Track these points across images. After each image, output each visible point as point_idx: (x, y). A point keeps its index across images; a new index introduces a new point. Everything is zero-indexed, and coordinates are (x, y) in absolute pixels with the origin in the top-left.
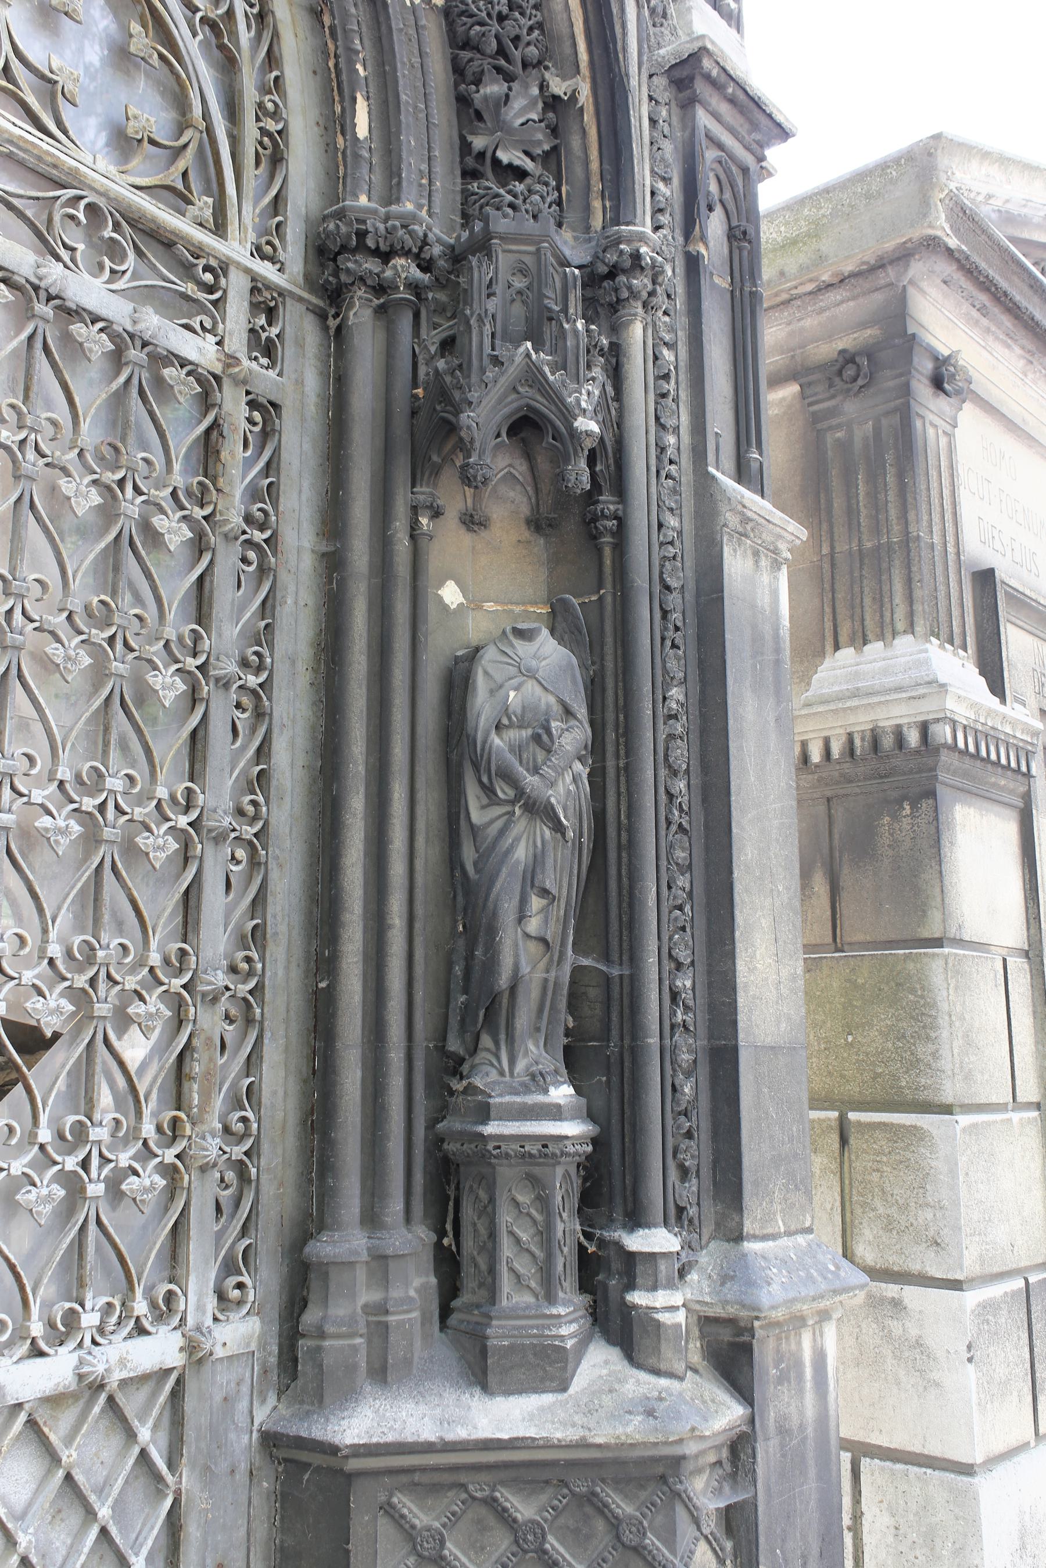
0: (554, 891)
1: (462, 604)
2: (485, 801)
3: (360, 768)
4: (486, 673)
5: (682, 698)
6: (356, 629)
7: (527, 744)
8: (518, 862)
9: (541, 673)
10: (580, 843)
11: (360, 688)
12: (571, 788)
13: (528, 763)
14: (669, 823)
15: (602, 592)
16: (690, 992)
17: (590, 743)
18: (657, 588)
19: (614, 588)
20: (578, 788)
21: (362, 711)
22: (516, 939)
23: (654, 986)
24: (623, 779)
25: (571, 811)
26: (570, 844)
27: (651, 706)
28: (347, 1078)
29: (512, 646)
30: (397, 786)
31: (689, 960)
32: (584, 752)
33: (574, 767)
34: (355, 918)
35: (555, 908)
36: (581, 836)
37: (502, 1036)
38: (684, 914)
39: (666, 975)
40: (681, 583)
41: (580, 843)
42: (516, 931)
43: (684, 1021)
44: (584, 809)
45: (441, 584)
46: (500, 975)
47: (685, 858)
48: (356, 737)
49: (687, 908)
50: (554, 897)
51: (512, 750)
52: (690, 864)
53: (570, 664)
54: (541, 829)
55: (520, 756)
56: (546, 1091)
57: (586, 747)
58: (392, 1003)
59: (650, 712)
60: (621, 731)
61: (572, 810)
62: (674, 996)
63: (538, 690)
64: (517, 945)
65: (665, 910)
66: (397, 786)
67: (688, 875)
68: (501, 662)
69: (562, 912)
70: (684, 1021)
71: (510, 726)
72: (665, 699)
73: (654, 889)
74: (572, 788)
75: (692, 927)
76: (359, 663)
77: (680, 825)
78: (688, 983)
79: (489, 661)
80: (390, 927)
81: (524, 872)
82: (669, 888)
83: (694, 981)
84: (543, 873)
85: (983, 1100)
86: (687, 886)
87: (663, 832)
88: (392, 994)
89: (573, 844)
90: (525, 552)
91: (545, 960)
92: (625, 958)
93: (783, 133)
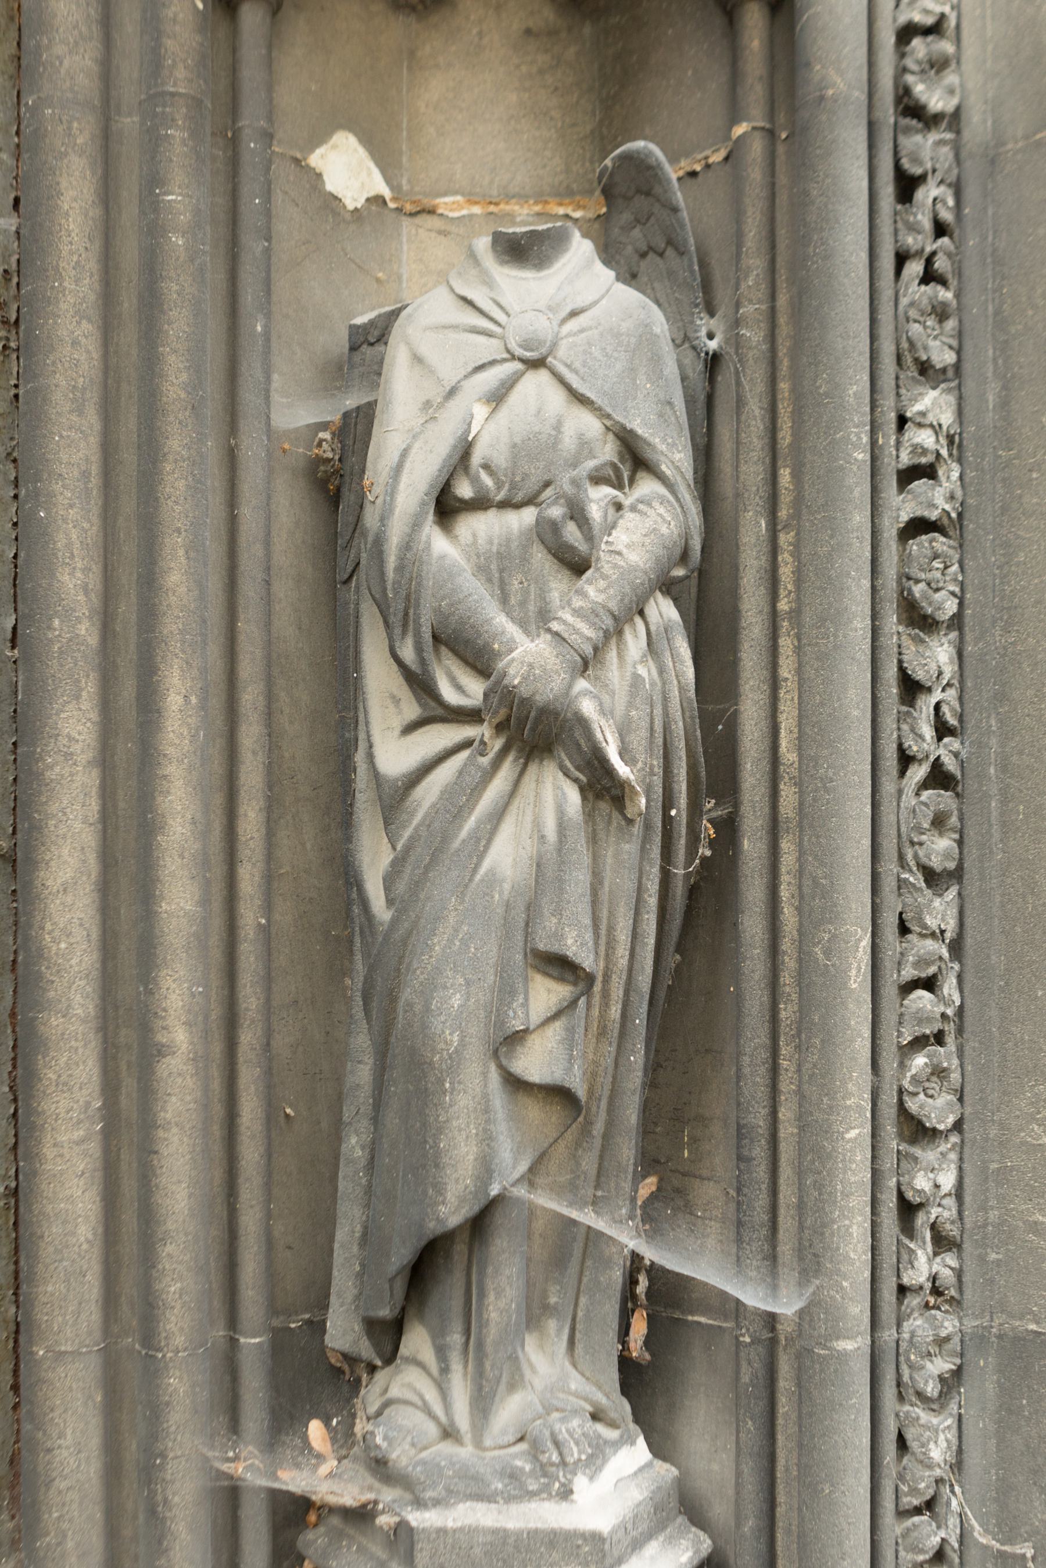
0: (587, 961)
1: (378, 200)
2: (412, 711)
3: (83, 629)
4: (417, 359)
5: (947, 418)
6: (65, 249)
7: (525, 548)
8: (493, 880)
9: (562, 352)
10: (668, 821)
11: (80, 412)
12: (642, 671)
13: (523, 603)
14: (906, 760)
15: (739, 130)
16: (951, 1202)
17: (696, 544)
18: (887, 113)
19: (771, 115)
20: (661, 671)
21: (86, 475)
22: (485, 1096)
23: (861, 1201)
24: (786, 644)
25: (638, 739)
26: (637, 829)
27: (865, 439)
28: (61, 1435)
29: (488, 282)
30: (176, 672)
31: (951, 1120)
32: (679, 572)
33: (651, 610)
34: (76, 1027)
35: (597, 999)
36: (668, 802)
37: (456, 1338)
38: (941, 999)
39: (889, 1163)
40: (954, 102)
41: (668, 821)
42: (485, 1074)
43: (934, 1278)
44: (679, 728)
45: (318, 138)
46: (440, 1189)
47: (947, 855)
48: (69, 545)
49: (949, 987)
50: (590, 979)
51: (482, 570)
52: (960, 867)
53: (646, 337)
54: (557, 787)
55: (503, 585)
56: (566, 1493)
57: (684, 557)
58: (169, 1248)
59: (862, 456)
60: (783, 514)
61: (644, 733)
62: (908, 1209)
63: (556, 399)
64: (487, 1111)
65: (889, 992)
66: (176, 672)
67: (951, 894)
68: (454, 327)
69: (615, 1012)
70: (934, 1278)
71: (480, 504)
72: (902, 421)
73: (866, 942)
74: (646, 671)
75: (960, 1031)
76: (75, 343)
77: (937, 764)
78: (948, 1180)
79: (426, 329)
80: (163, 1051)
81: (508, 906)
82: (904, 929)
83: (960, 1169)
84: (558, 912)
85: (396, 459)
86: (951, 926)
87: (888, 786)
88: (170, 1225)
89: (648, 827)
90: (543, 59)
91: (570, 1136)
92: (786, 1249)
93: (591, 1478)
